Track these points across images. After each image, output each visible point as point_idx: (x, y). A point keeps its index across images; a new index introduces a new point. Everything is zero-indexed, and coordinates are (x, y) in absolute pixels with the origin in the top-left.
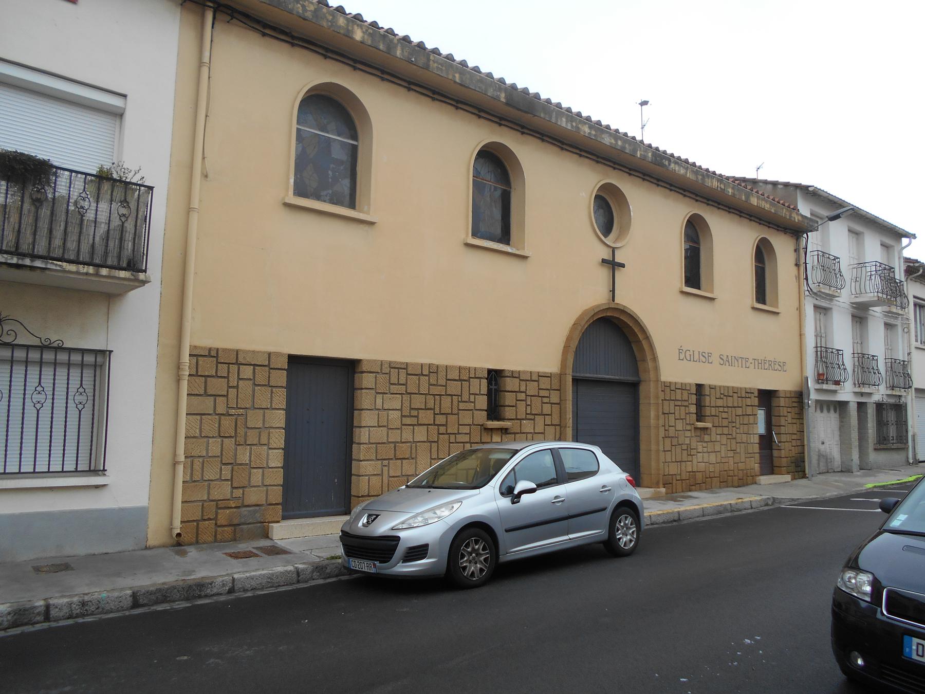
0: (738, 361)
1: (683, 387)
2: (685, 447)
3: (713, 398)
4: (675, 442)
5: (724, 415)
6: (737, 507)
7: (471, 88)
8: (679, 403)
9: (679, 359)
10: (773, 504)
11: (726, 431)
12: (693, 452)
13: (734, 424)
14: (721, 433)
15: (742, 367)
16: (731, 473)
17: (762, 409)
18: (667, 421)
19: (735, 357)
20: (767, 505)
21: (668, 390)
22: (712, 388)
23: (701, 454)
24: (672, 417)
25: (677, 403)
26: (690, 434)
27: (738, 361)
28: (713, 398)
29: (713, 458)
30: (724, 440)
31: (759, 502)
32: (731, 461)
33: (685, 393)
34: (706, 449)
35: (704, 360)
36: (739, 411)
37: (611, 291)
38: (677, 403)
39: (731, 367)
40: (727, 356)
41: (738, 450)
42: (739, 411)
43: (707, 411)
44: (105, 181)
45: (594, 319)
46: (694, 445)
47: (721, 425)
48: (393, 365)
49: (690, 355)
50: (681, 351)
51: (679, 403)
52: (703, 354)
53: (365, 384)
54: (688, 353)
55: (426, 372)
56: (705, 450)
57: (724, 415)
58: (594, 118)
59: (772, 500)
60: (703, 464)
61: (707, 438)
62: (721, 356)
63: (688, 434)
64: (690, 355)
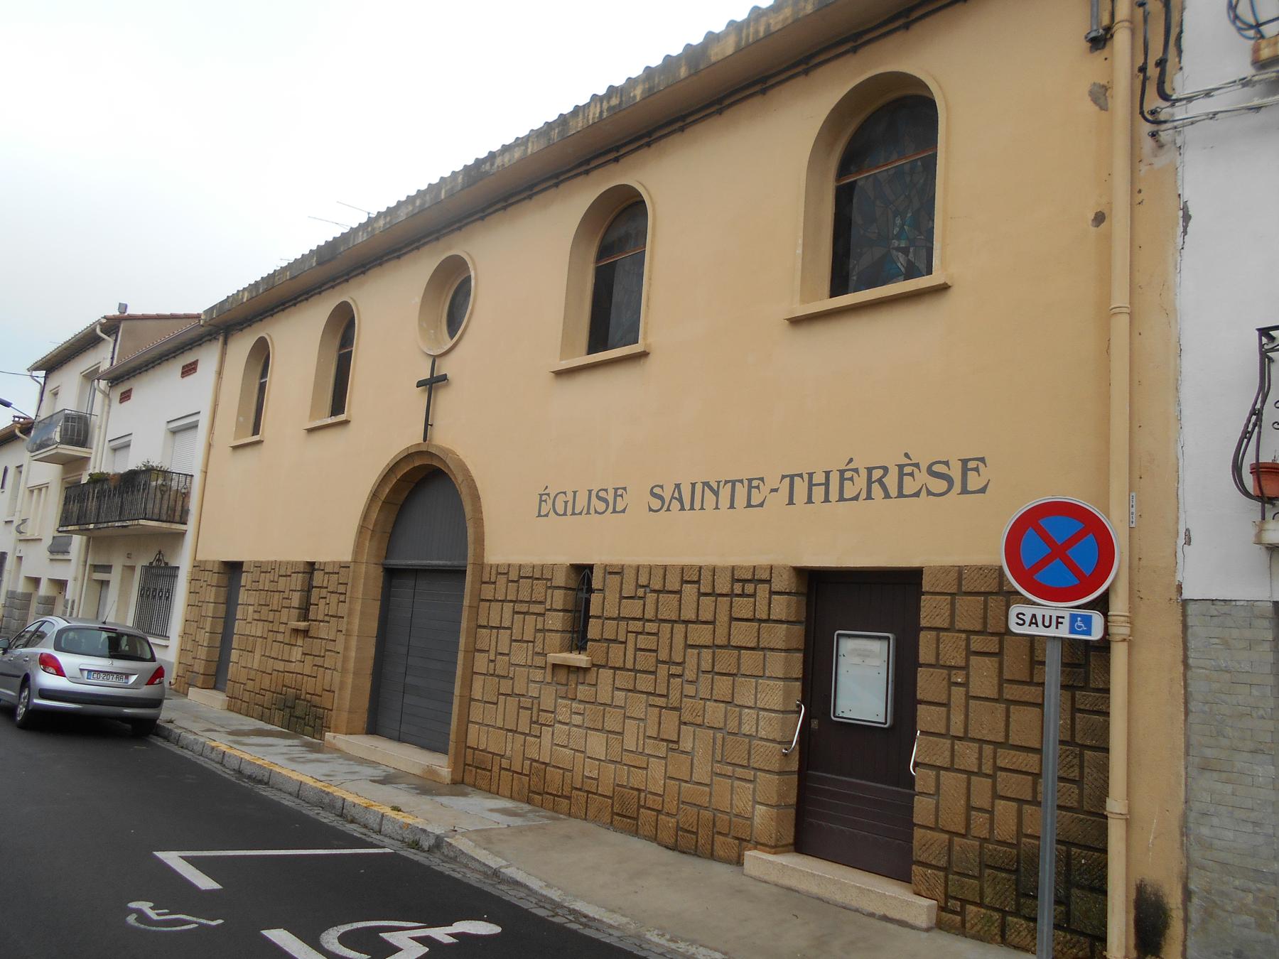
0: (716, 493)
1: (539, 575)
2: (526, 702)
3: (612, 597)
4: (505, 687)
5: (643, 642)
6: (353, 811)
7: (299, 274)
8: (524, 608)
9: (539, 515)
10: (430, 850)
11: (645, 683)
12: (544, 717)
13: (675, 670)
14: (651, 689)
15: (732, 507)
16: (651, 801)
17: (880, 638)
18: (493, 643)
19: (706, 484)
20: (416, 845)
21: (689, 590)
22: (616, 572)
23: (567, 727)
24: (504, 635)
25: (519, 607)
26: (542, 676)
27: (716, 493)
28: (612, 597)
29: (597, 745)
30: (638, 706)
31: (401, 828)
32: (657, 769)
33: (540, 587)
34: (579, 718)
35: (601, 506)
36: (701, 634)
37: (431, 425)
38: (519, 607)
39: (687, 513)
40: (678, 486)
41: (687, 745)
42: (701, 634)
43: (594, 630)
44: (144, 469)
45: (398, 477)
46: (547, 703)
47: (629, 665)
48: (609, 569)
49: (566, 503)
50: (544, 498)
51: (524, 608)
52: (602, 494)
53: (559, 594)
54: (561, 498)
55: (673, 583)
56: (577, 719)
57: (643, 642)
58: (403, 198)
59: (432, 841)
60: (567, 751)
61: (583, 691)
62: (656, 490)
63: (538, 675)
64: (566, 503)
